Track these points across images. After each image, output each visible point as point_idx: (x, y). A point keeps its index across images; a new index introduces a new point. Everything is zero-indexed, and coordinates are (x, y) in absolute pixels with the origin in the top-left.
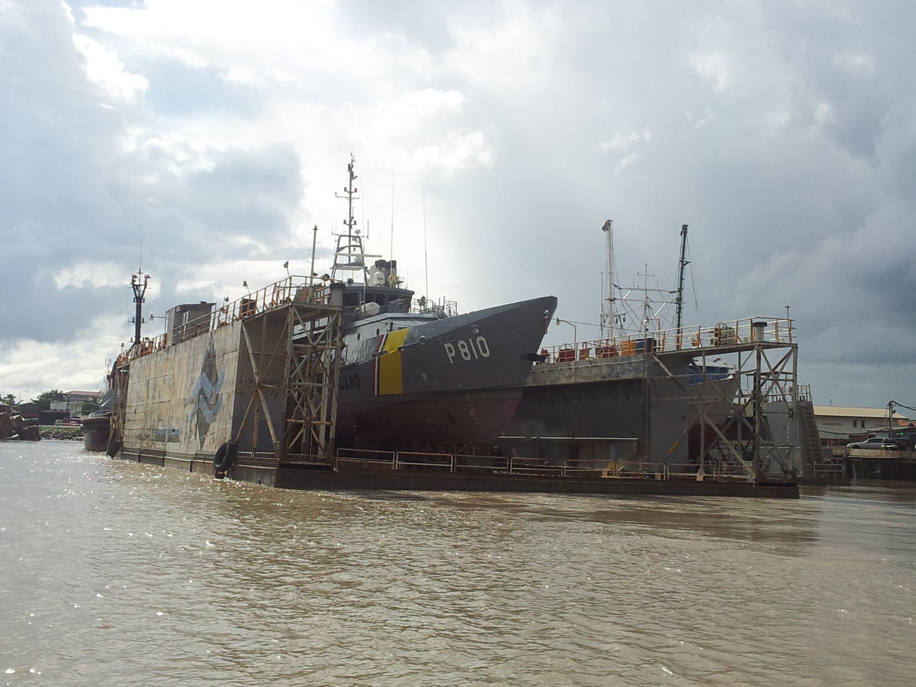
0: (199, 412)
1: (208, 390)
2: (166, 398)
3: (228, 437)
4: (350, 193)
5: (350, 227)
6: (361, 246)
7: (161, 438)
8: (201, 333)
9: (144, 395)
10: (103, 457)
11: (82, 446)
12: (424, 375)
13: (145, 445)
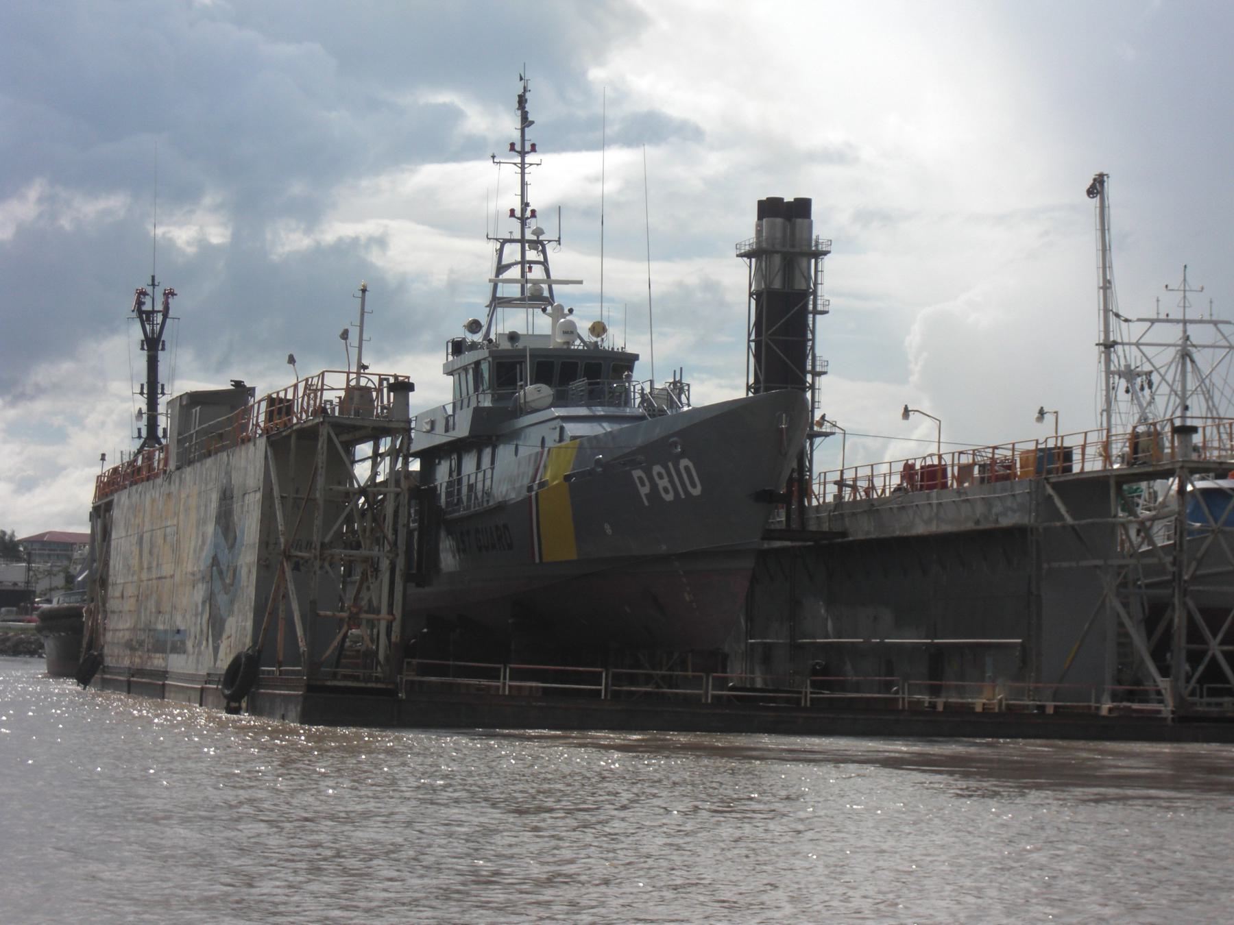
0: (210, 598)
1: (224, 558)
2: (167, 569)
3: (248, 641)
6: (545, 263)
7: (161, 647)
8: (217, 451)
9: (135, 562)
10: (70, 685)
11: (44, 669)
12: (607, 527)
13: (137, 660)
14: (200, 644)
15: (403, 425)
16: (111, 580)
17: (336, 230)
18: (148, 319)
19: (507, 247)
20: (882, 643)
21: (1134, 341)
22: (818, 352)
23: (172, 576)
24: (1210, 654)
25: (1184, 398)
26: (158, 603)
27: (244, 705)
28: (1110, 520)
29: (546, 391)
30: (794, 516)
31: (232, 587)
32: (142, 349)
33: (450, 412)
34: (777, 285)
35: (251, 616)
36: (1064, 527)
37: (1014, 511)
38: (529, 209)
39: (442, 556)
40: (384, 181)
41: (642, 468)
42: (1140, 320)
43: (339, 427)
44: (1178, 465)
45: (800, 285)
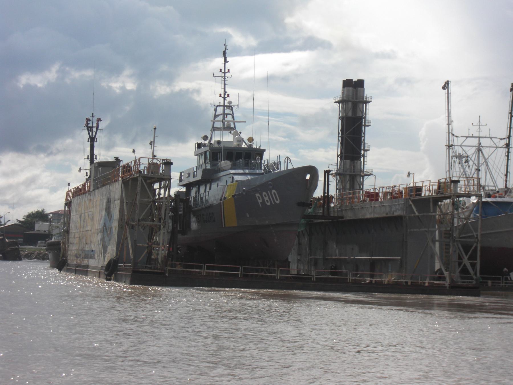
0: (103, 239)
1: (107, 225)
2: (89, 228)
3: (115, 254)
4: (225, 73)
5: (225, 100)
9: (78, 224)
11: (49, 265)
12: (247, 214)
13: (79, 261)
14: (99, 255)
15: (168, 177)
16: (70, 231)
17: (182, 85)
18: (91, 130)
19: (218, 108)
20: (354, 258)
21: (460, 144)
22: (366, 142)
23: (91, 230)
24: (463, 263)
25: (478, 166)
26: (86, 240)
27: (113, 278)
28: (430, 214)
29: (229, 163)
30: (325, 210)
31: (110, 235)
32: (88, 141)
33: (195, 170)
34: (350, 114)
35: (116, 245)
36: (414, 216)
37: (399, 210)
38: (227, 94)
39: (192, 224)
40: (200, 64)
41: (259, 193)
42: (462, 137)
43: (146, 178)
44: (452, 194)
45: (359, 114)
